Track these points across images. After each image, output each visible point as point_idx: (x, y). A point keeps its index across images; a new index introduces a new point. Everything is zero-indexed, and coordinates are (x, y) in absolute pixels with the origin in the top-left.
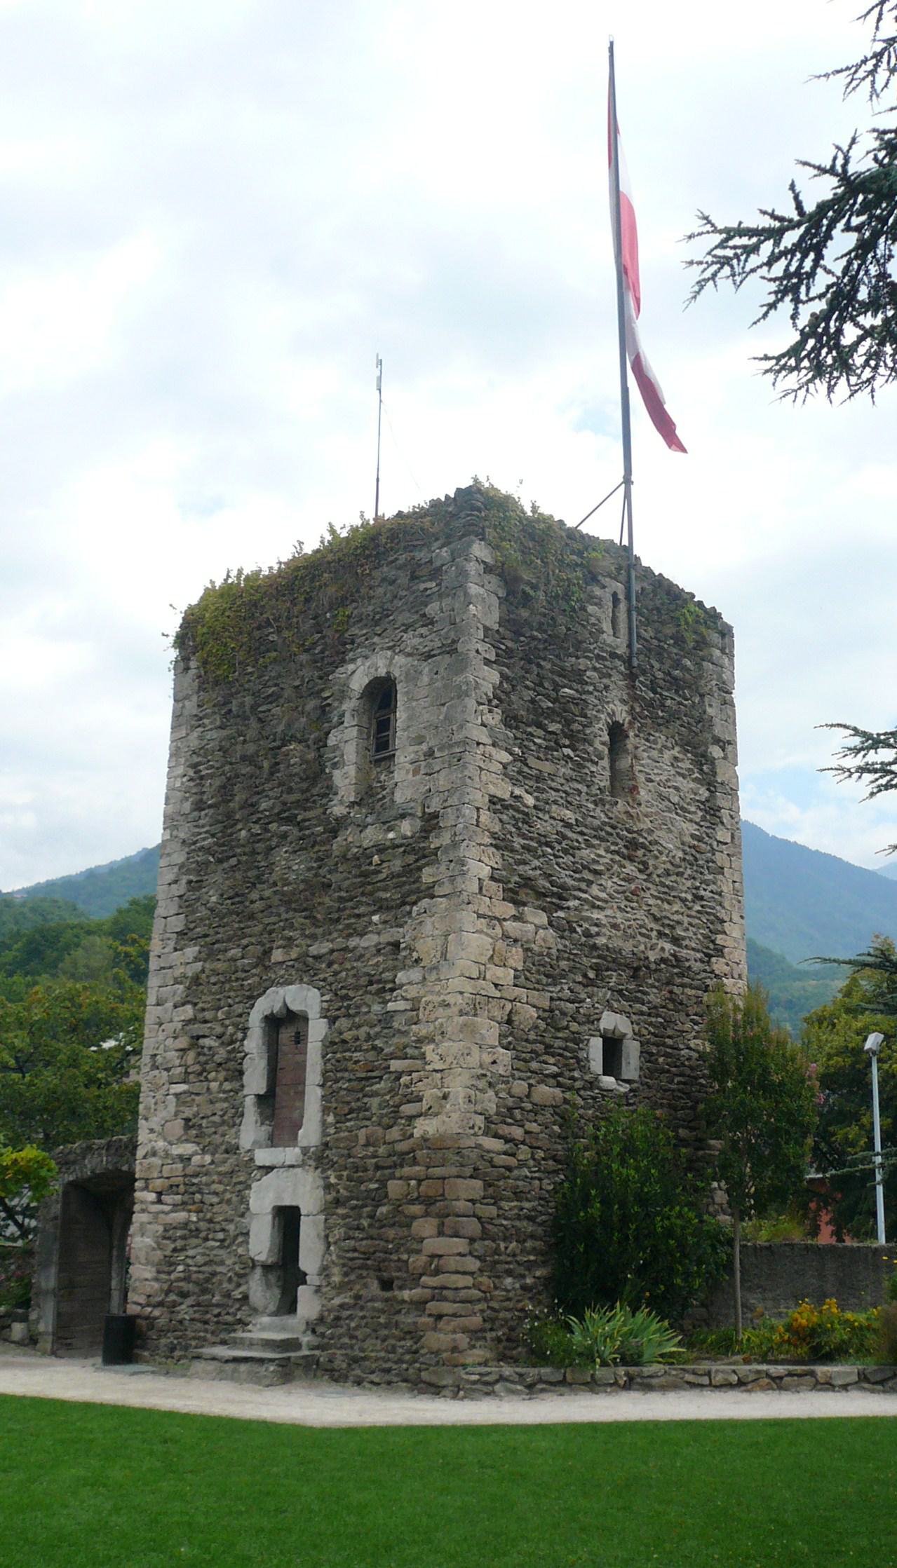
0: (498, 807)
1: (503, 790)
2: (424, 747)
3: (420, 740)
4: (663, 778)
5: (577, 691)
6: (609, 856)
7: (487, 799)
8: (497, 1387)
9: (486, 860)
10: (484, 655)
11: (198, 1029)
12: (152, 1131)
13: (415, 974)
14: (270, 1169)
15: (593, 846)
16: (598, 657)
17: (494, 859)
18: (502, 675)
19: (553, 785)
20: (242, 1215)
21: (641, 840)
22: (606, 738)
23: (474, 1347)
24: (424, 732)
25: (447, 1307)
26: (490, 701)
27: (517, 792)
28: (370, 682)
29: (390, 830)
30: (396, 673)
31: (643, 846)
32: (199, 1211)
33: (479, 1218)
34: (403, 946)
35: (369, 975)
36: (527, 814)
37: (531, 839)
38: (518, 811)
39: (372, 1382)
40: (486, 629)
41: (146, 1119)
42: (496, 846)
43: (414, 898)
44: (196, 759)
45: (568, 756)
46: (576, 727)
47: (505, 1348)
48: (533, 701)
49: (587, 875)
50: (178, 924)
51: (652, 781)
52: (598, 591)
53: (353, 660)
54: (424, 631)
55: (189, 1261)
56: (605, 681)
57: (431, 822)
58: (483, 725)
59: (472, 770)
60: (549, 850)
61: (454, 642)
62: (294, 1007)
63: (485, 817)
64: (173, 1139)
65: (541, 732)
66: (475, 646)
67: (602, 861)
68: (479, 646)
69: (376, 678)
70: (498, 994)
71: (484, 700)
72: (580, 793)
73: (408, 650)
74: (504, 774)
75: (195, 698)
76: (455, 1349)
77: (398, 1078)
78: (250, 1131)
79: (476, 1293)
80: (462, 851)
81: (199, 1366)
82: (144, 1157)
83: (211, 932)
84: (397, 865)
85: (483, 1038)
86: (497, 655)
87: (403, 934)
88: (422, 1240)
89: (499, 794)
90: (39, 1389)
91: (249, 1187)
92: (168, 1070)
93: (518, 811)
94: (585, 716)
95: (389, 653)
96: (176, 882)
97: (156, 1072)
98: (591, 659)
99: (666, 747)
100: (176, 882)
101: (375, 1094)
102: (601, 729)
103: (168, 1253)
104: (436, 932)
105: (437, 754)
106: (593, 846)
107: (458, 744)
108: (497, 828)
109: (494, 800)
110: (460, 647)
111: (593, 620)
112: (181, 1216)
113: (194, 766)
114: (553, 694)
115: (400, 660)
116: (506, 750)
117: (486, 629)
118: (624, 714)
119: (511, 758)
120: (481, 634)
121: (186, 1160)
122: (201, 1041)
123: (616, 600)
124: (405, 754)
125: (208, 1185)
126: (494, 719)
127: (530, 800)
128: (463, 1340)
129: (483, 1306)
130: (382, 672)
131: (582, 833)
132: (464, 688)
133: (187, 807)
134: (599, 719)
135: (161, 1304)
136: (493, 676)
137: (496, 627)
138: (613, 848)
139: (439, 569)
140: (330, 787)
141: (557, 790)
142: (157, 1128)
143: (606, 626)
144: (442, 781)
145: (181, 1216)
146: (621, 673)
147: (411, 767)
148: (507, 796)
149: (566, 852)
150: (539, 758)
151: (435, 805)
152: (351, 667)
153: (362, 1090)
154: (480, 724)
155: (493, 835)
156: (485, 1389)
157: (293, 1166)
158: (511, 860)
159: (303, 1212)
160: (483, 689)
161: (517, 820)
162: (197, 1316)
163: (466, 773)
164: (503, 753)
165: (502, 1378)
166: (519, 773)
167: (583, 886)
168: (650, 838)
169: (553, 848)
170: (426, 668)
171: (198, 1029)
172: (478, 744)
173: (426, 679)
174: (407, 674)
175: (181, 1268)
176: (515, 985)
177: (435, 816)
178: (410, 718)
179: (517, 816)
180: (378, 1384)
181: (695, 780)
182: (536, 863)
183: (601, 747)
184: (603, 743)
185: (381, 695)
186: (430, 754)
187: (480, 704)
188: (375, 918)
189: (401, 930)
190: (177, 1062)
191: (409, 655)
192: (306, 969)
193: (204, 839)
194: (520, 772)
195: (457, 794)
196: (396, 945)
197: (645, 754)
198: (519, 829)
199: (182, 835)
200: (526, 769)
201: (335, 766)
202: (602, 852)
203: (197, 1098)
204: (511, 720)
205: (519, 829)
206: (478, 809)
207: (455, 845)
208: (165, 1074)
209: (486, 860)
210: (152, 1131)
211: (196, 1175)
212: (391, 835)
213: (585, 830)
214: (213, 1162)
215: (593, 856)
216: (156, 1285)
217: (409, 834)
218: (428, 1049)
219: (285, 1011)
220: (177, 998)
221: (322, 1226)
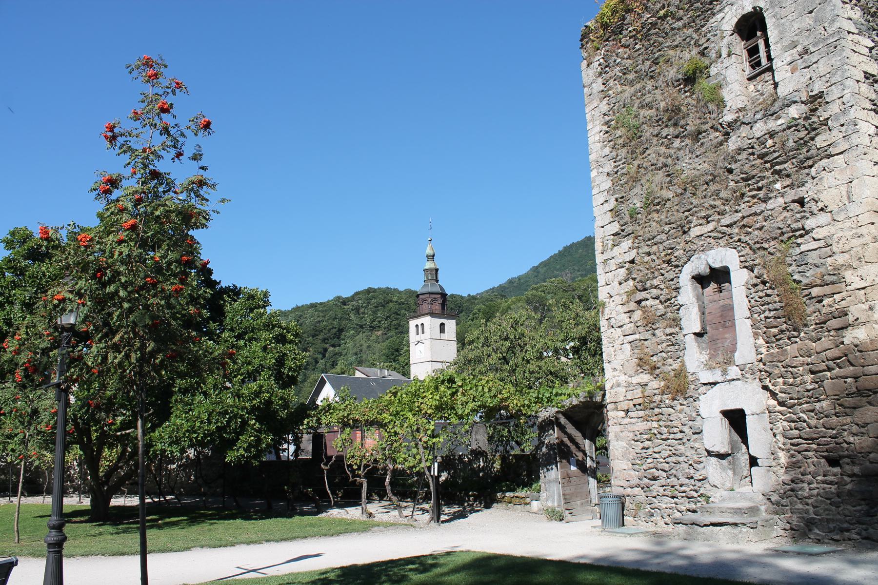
2: (800, 48)
11: (640, 296)
12: (615, 369)
13: (823, 218)
24: (796, 38)
28: (739, 20)
34: (806, 200)
35: (780, 228)
39: (832, 539)
41: (609, 362)
43: (810, 162)
53: (721, 11)
55: (657, 456)
57: (816, 100)
62: (717, 265)
64: (632, 373)
69: (744, 16)
77: (820, 301)
78: (695, 358)
82: (612, 388)
87: (808, 191)
90: (173, 532)
104: (839, 182)
107: (832, 35)
113: (607, 123)
122: (643, 303)
133: (607, 150)
135: (638, 486)
142: (619, 367)
144: (822, 68)
147: (788, 68)
152: (719, 16)
163: (844, 54)
171: (640, 296)
172: (849, 33)
177: (821, 95)
178: (781, 32)
180: (837, 541)
189: (803, 188)
192: (721, 236)
195: (839, 73)
196: (801, 202)
203: (646, 343)
210: (615, 369)
216: (633, 473)
217: (797, 117)
218: (848, 275)
219: (708, 270)
220: (621, 278)
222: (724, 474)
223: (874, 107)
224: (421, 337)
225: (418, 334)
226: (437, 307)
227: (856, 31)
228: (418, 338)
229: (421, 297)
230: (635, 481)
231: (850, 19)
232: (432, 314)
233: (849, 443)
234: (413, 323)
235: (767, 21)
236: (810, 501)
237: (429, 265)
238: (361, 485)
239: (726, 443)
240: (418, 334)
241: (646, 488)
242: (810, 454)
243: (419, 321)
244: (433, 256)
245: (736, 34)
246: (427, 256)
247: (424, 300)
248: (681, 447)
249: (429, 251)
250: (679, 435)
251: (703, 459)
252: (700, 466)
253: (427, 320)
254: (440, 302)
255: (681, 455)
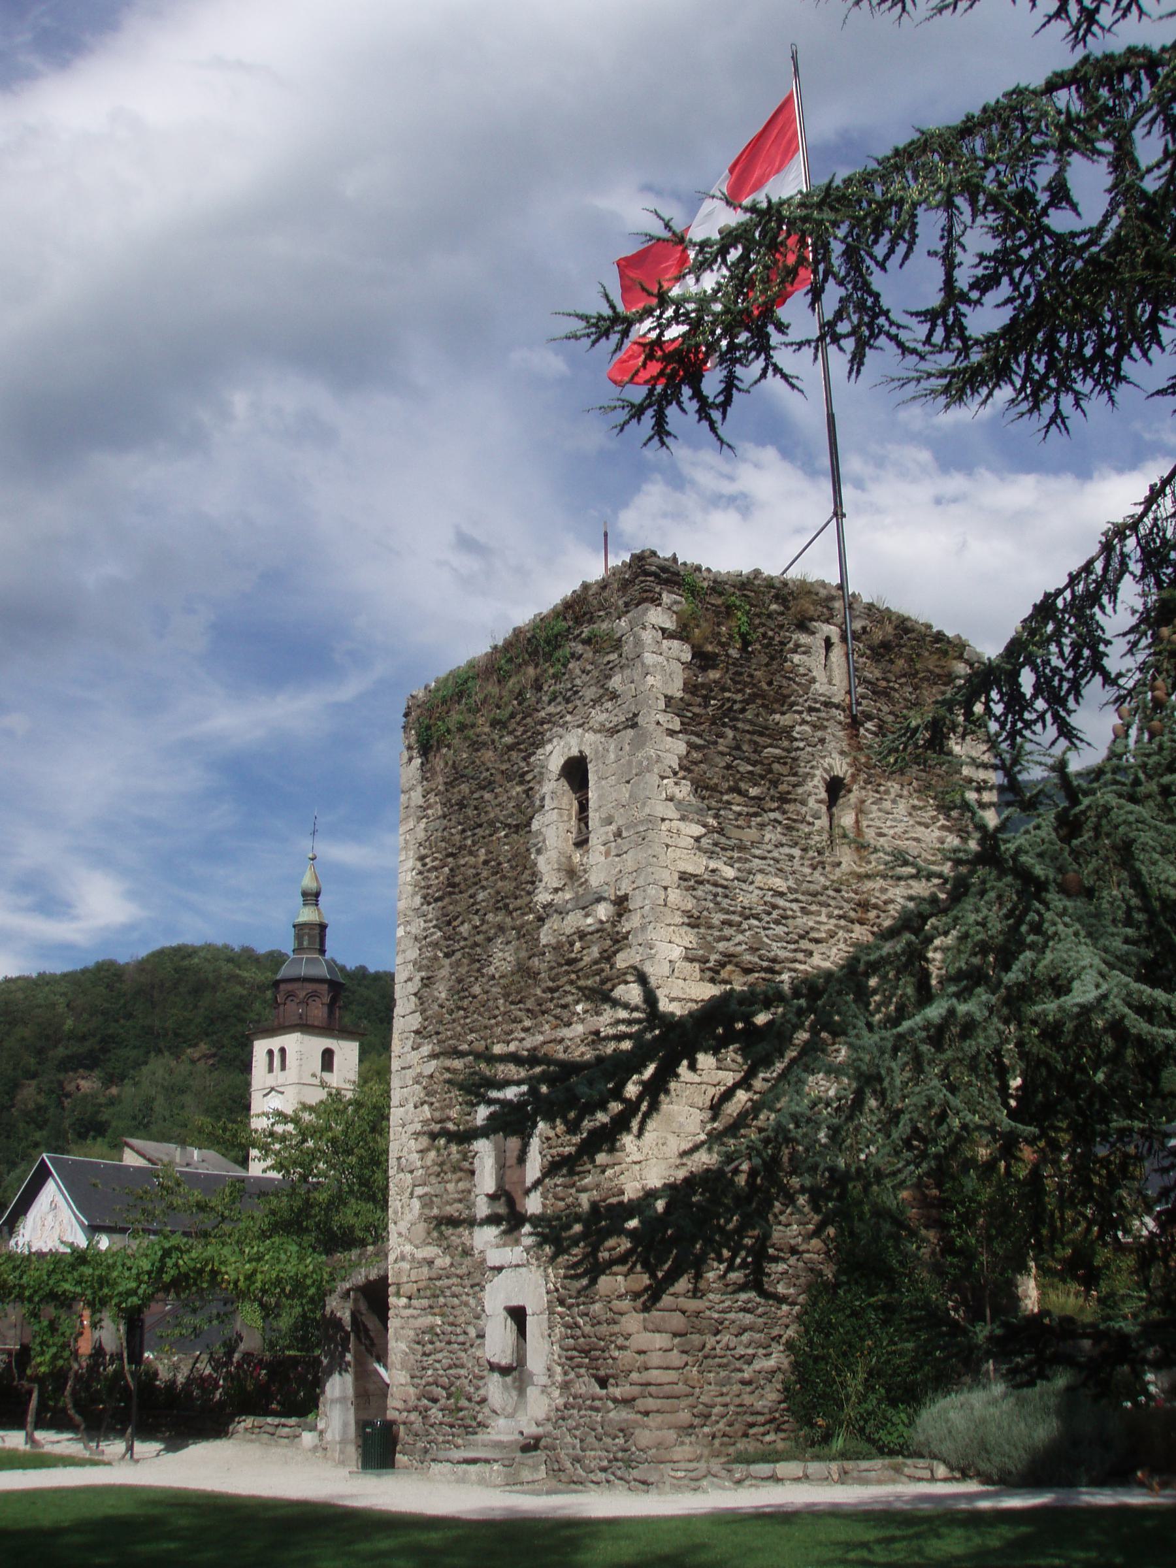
0: (692, 883)
1: (697, 865)
2: (613, 827)
3: (609, 821)
4: (899, 830)
5: (783, 749)
6: (833, 921)
7: (676, 876)
8: (704, 1483)
9: (678, 940)
10: (666, 725)
14: (499, 1269)
15: (812, 913)
16: (811, 710)
17: (689, 938)
18: (689, 744)
19: (757, 852)
20: (478, 1317)
21: (874, 901)
22: (824, 795)
23: (682, 1443)
25: (651, 1403)
26: (675, 773)
27: (713, 865)
29: (587, 915)
30: (587, 752)
31: (875, 907)
32: (442, 1315)
33: (684, 1312)
36: (725, 887)
37: (734, 913)
38: (716, 885)
40: (669, 699)
42: (689, 925)
44: (423, 851)
45: (775, 820)
46: (783, 787)
47: (722, 1444)
48: (728, 767)
49: (805, 944)
50: (415, 1021)
51: (884, 835)
52: (804, 639)
53: (550, 741)
54: (609, 705)
55: (438, 1365)
56: (819, 734)
57: (621, 904)
58: (670, 799)
59: (659, 850)
60: (755, 922)
61: (635, 715)
63: (674, 896)
65: (738, 799)
66: (656, 717)
67: (823, 928)
68: (661, 717)
70: (697, 1079)
71: (669, 773)
72: (791, 857)
73: (597, 726)
74: (699, 849)
75: (419, 789)
76: (659, 1445)
77: (603, 1172)
79: (681, 1388)
80: (651, 934)
81: (436, 1468)
82: (396, 1261)
83: (441, 1029)
84: (595, 952)
85: (681, 1125)
86: (682, 723)
88: (627, 1337)
89: (690, 869)
91: (483, 1289)
92: (411, 1172)
93: (716, 885)
94: (795, 774)
95: (580, 730)
96: (410, 979)
97: (402, 1175)
98: (800, 713)
99: (901, 796)
100: (410, 979)
101: (584, 1190)
102: (815, 787)
103: (419, 1357)
105: (624, 834)
106: (812, 913)
108: (689, 904)
109: (684, 876)
110: (639, 719)
111: (802, 670)
112: (429, 1320)
113: (422, 858)
114: (755, 757)
115: (590, 737)
116: (698, 822)
117: (669, 699)
118: (845, 767)
119: (703, 830)
120: (662, 704)
121: (430, 1263)
123: (828, 644)
124: (599, 834)
125: (449, 1288)
126: (684, 791)
127: (730, 873)
128: (672, 1435)
129: (691, 1400)
130: (575, 752)
131: (796, 900)
132: (645, 763)
134: (814, 776)
135: (416, 1408)
136: (679, 746)
137: (679, 694)
138: (836, 912)
139: (619, 640)
140: (534, 874)
141: (764, 858)
142: (404, 1231)
143: (819, 673)
145: (429, 1320)
146: (840, 723)
148: (700, 870)
149: (777, 922)
150: (738, 827)
151: (625, 888)
152: (549, 747)
153: (574, 1185)
154: (665, 797)
155: (687, 913)
156: (693, 1484)
157: (518, 1266)
158: (709, 938)
159: (529, 1311)
160: (667, 762)
161: (716, 895)
162: (446, 1419)
164: (693, 826)
165: (709, 1473)
166: (718, 841)
167: (800, 956)
168: (884, 897)
169: (760, 920)
170: (612, 744)
172: (663, 820)
173: (612, 756)
174: (597, 752)
175: (430, 1372)
176: (719, 1068)
177: (625, 898)
178: (600, 797)
179: (714, 890)
180: (598, 1483)
181: (943, 828)
182: (740, 938)
183: (816, 806)
184: (820, 802)
185: (576, 772)
186: (618, 834)
187: (663, 778)
188: (579, 1008)
190: (419, 1164)
191: (595, 732)
193: (432, 934)
194: (716, 844)
197: (875, 807)
198: (717, 904)
199: (414, 931)
200: (723, 840)
201: (539, 852)
202: (823, 918)
204: (701, 787)
205: (717, 904)
206: (666, 888)
207: (643, 928)
208: (409, 1176)
209: (678, 940)
210: (400, 1234)
211: (439, 1278)
212: (590, 921)
213: (801, 897)
214: (452, 1265)
215: (811, 924)
221: (545, 1325)
222: (506, 1395)
223: (686, 920)
224: (278, 1077)
225: (271, 1070)
226: (318, 1011)
227: (677, 815)
228: (271, 1080)
229: (283, 987)
230: (412, 1402)
231: (671, 800)
232: (306, 1027)
233: (614, 1359)
234: (260, 1048)
235: (590, 776)
236: (578, 1433)
237: (307, 915)
238: (30, 1393)
239: (509, 1352)
240: (271, 1070)
241: (424, 1413)
242: (582, 1371)
243: (275, 1043)
244: (317, 895)
245: (563, 781)
246: (305, 894)
247: (290, 995)
248: (463, 1354)
249: (308, 882)
250: (461, 1338)
251: (485, 1373)
252: (481, 1383)
253: (292, 1042)
254: (327, 1000)
255: (462, 1366)
